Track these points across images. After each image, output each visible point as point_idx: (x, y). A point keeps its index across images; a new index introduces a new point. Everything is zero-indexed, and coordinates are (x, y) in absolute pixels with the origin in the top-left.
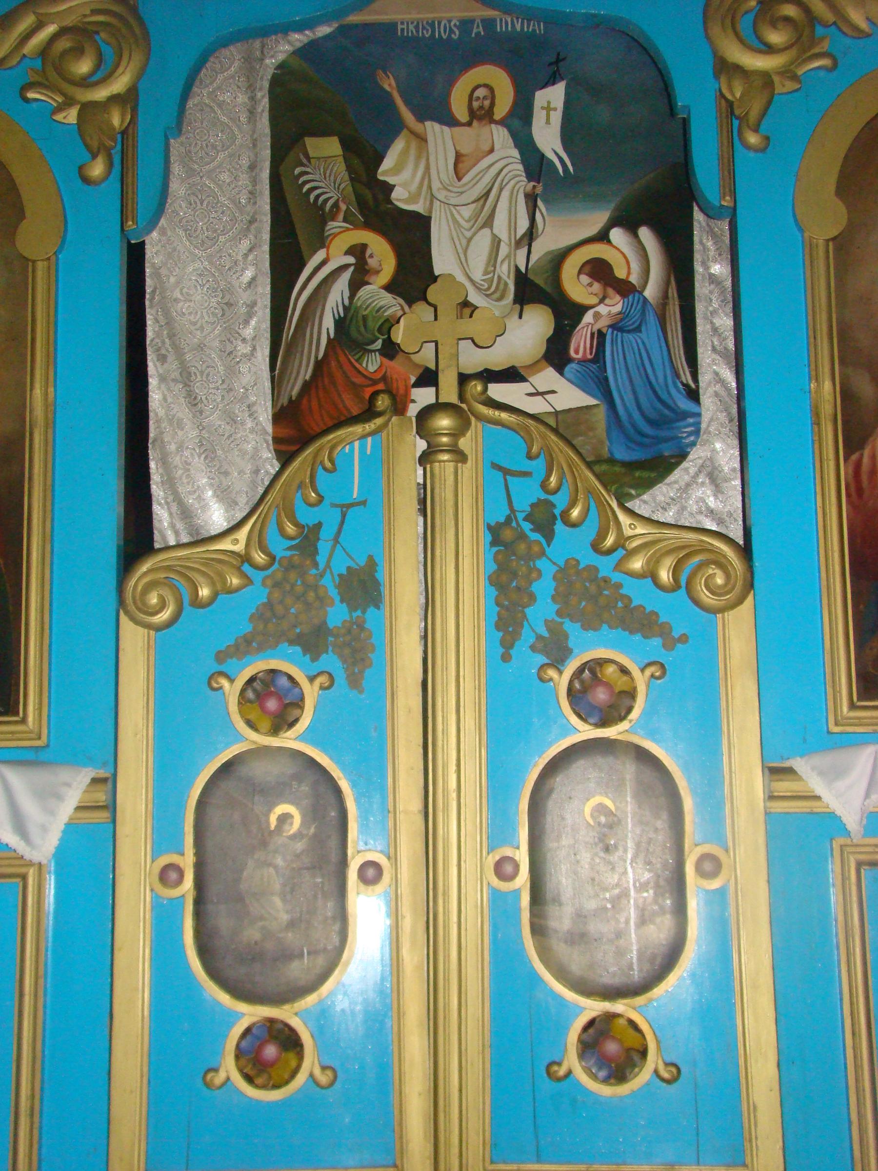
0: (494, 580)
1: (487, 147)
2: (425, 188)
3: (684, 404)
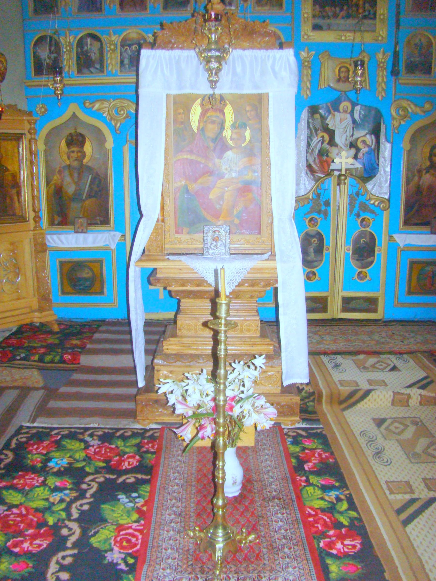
0: (349, 204)
3: (376, 166)
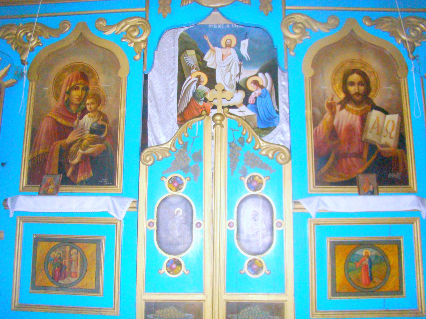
1: (229, 53)
2: (215, 62)
3: (275, 115)
